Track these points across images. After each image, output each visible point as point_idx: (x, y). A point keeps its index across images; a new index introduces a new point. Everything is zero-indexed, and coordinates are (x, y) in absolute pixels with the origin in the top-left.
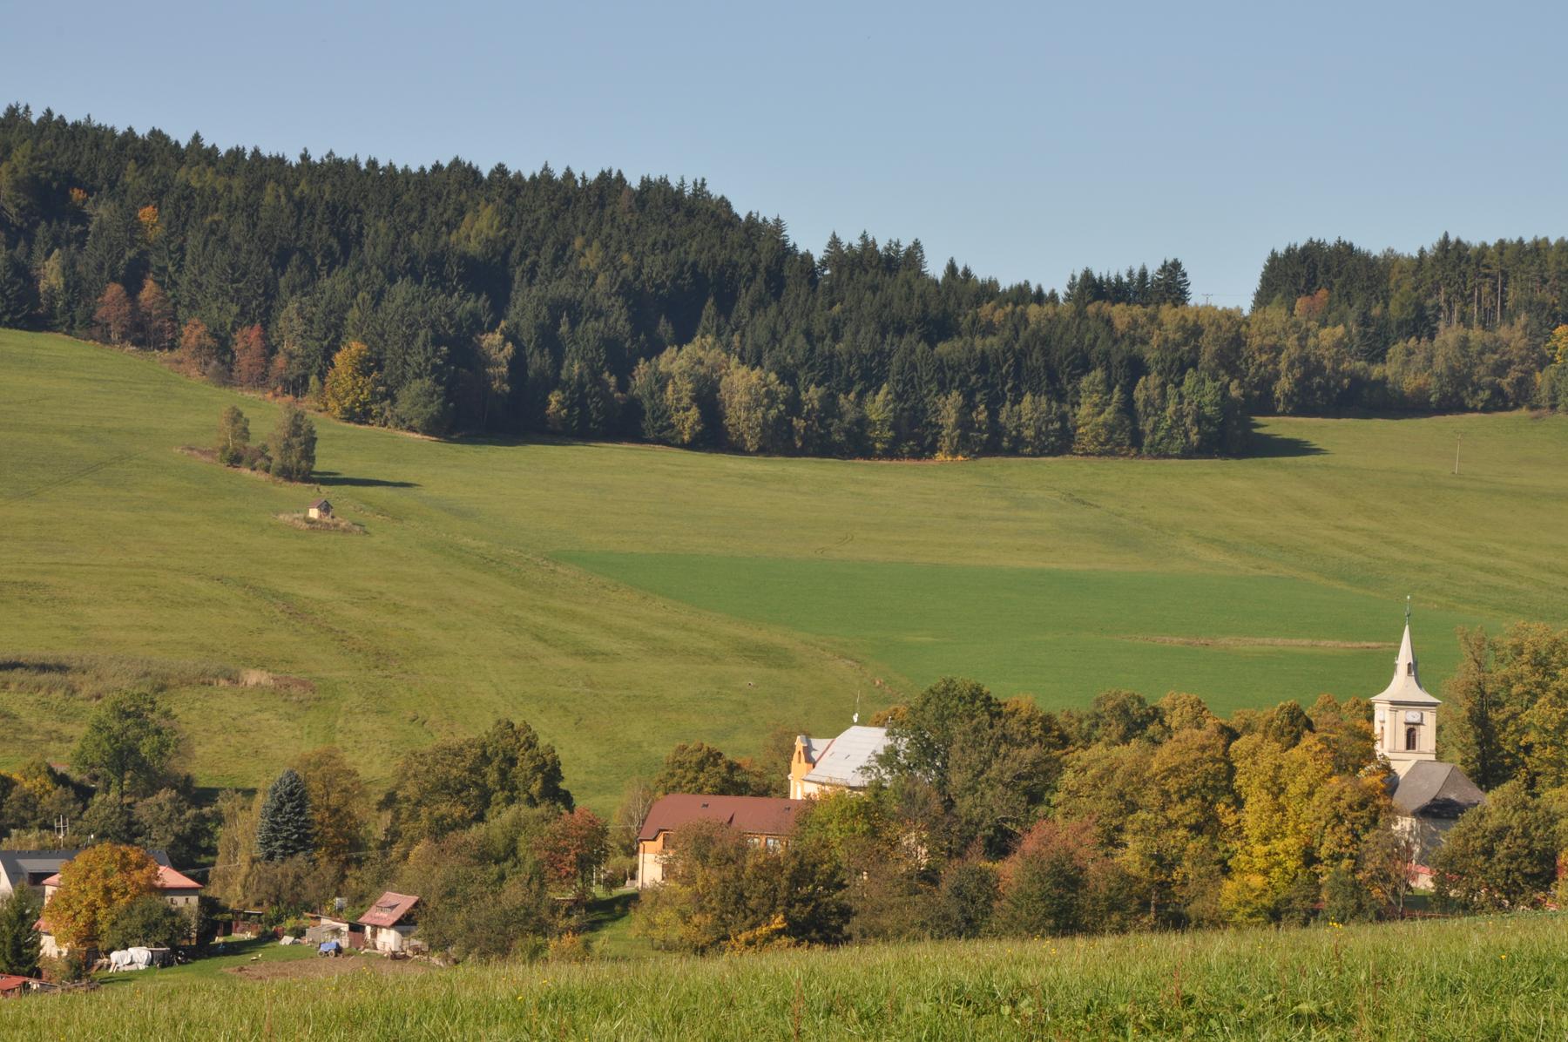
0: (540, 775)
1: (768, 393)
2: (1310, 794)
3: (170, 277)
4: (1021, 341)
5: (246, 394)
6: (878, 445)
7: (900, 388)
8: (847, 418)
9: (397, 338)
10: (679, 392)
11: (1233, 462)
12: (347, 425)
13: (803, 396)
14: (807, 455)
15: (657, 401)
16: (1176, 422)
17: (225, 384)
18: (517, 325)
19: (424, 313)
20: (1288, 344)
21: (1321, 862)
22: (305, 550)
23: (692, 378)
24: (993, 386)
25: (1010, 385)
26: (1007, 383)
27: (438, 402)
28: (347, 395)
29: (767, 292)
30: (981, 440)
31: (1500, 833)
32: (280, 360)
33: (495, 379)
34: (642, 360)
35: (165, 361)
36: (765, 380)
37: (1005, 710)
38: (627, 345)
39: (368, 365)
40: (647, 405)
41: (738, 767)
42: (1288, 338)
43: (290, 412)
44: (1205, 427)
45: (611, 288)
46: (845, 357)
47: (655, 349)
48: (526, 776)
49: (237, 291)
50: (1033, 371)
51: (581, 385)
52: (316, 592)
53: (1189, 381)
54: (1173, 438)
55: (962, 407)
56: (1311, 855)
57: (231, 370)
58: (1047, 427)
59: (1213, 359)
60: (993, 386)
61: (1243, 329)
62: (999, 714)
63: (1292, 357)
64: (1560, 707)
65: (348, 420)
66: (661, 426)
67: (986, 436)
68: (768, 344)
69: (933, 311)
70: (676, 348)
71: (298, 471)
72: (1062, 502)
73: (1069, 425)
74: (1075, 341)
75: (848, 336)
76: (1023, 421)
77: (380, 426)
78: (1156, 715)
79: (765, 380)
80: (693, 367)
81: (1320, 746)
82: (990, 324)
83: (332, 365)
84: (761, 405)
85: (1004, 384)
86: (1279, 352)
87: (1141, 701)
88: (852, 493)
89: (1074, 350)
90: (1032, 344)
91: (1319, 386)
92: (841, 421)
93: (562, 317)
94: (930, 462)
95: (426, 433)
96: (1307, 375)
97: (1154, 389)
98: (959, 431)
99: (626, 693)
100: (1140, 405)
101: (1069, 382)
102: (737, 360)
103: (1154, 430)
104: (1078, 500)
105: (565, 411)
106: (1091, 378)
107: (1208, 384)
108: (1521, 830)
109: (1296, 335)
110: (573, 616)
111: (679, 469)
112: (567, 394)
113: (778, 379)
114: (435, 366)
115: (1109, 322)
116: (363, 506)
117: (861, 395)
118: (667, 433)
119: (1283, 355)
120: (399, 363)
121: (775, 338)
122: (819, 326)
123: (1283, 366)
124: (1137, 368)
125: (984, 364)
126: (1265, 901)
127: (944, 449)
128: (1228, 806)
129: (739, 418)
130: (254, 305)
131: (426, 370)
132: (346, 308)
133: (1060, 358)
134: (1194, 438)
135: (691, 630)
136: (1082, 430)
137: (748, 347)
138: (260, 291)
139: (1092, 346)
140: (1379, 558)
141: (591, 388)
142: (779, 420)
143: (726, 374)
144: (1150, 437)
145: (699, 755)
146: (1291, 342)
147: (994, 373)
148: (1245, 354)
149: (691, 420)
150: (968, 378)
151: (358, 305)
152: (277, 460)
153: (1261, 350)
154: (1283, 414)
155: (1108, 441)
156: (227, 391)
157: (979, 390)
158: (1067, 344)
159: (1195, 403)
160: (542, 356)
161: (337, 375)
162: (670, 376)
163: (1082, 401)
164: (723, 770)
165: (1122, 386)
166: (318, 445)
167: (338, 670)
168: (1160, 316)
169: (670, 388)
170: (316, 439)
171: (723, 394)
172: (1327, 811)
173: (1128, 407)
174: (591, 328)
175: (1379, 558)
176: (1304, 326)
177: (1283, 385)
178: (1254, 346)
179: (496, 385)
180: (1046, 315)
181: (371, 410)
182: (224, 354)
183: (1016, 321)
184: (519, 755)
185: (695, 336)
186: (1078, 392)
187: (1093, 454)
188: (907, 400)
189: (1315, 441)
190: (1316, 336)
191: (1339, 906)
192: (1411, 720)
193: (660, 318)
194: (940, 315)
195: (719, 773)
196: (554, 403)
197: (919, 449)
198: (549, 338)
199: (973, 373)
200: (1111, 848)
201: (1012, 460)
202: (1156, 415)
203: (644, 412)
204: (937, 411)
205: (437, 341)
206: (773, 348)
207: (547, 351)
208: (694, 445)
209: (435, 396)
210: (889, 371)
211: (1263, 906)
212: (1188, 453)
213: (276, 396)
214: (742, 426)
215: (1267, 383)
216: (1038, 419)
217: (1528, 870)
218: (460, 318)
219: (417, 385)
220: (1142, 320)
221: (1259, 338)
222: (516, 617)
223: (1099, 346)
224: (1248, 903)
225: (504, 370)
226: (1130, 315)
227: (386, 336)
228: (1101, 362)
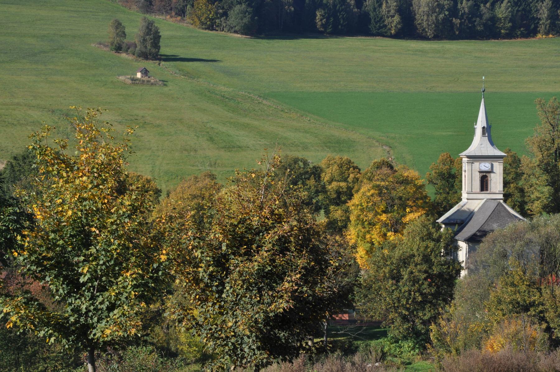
5: (157, 17)
6: (503, 31)
8: (484, 18)
14: (463, 38)
15: (377, 13)
22: (119, 95)
27: (248, 16)
31: (405, 261)
40: (372, 15)
43: (145, 22)
55: (551, 8)
66: (379, 26)
77: (221, 31)
81: (372, 191)
88: (476, 57)
94: (533, 39)
95: (242, 34)
98: (549, 21)
110: (245, 126)
112: (326, 11)
117: (493, 5)
118: (383, 30)
127: (541, 32)
129: (422, 20)
169: (384, 5)
197: (526, 32)
203: (370, 19)
204: (537, 11)
208: (398, 36)
209: (247, 14)
213: (171, 17)
214: (425, 24)
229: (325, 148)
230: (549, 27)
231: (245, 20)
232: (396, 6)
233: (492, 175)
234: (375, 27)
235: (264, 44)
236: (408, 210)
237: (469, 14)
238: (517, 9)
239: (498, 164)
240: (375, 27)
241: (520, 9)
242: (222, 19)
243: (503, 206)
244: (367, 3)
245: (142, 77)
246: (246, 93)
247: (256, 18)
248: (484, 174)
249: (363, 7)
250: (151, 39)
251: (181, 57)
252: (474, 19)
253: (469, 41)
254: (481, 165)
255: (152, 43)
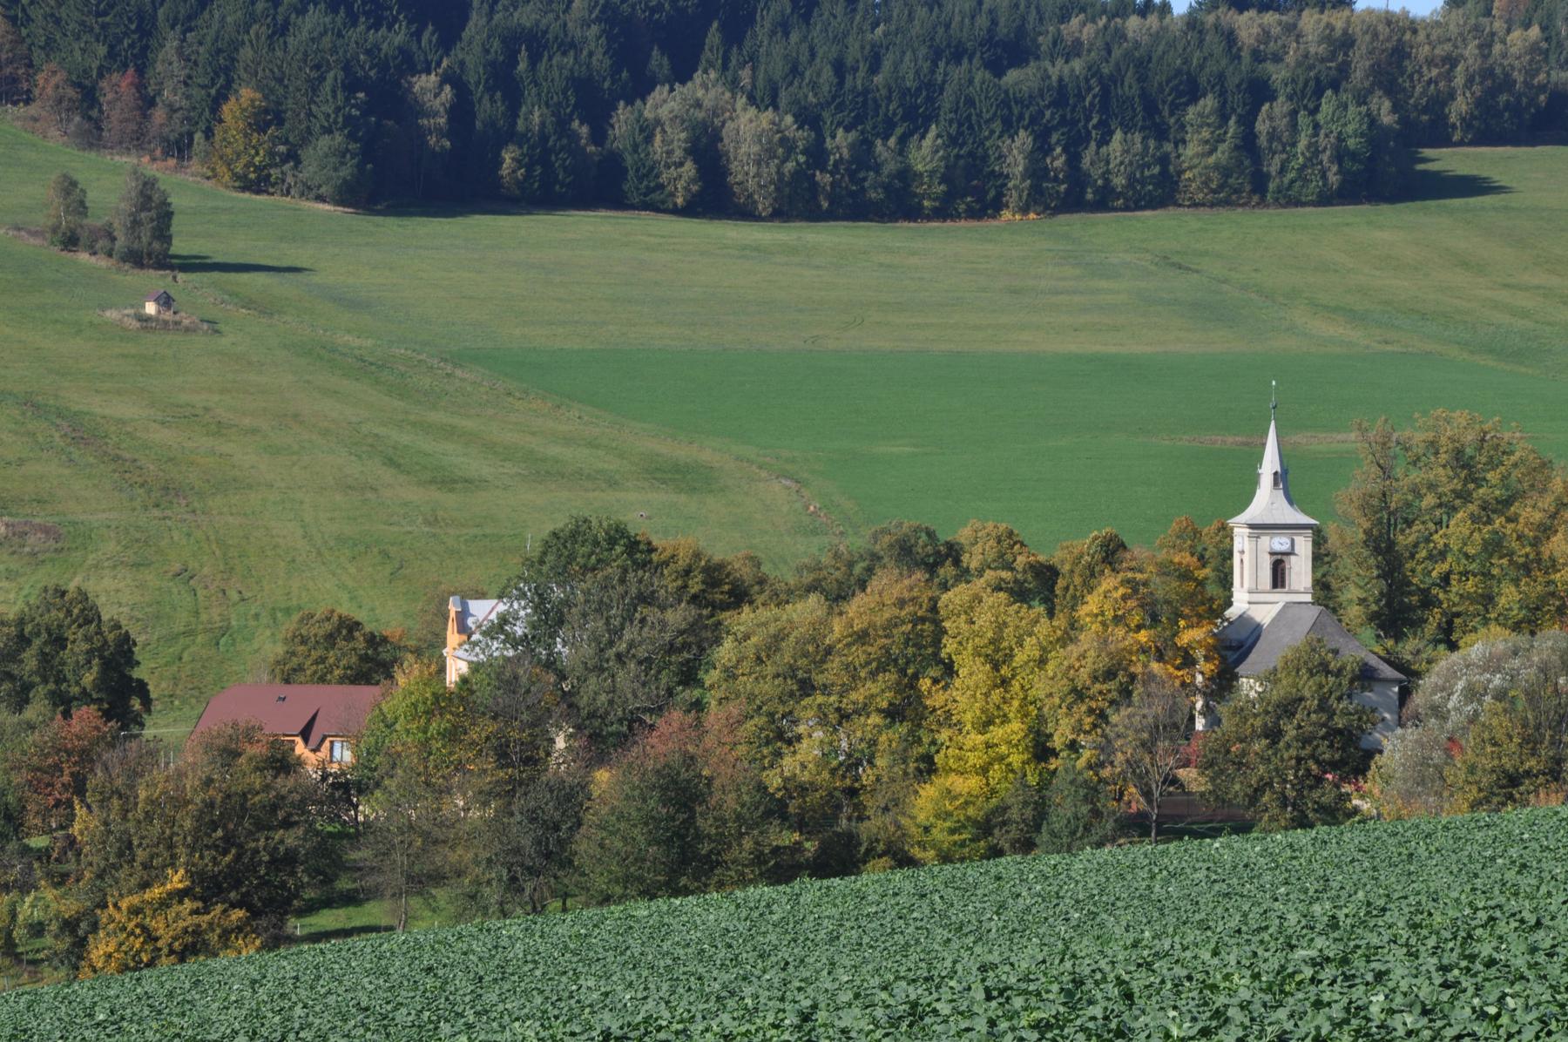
0: (96, 661)
1: (783, 141)
2: (1042, 662)
3: (24, 10)
4: (1113, 60)
5: (117, 158)
6: (926, 203)
7: (953, 130)
8: (886, 170)
9: (299, 82)
10: (671, 143)
11: (1385, 208)
12: (241, 195)
13: (829, 144)
15: (642, 155)
16: (1310, 159)
17: (91, 146)
18: (462, 63)
19: (334, 50)
20: (1467, 53)
21: (1056, 755)
22: (124, 356)
23: (686, 124)
24: (1074, 122)
25: (1095, 121)
26: (1092, 118)
28: (239, 156)
29: (792, 13)
30: (1058, 192)
32: (159, 115)
33: (431, 133)
34: (622, 103)
35: (18, 118)
36: (778, 125)
37: (654, 557)
38: (606, 85)
39: (265, 119)
40: (629, 160)
41: (385, 640)
42: (1466, 46)
43: (137, 179)
44: (1348, 164)
45: (591, 12)
46: (884, 92)
47: (641, 88)
48: (78, 662)
49: (104, 26)
50: (1124, 102)
51: (544, 138)
52: (126, 409)
53: (1327, 106)
54: (1306, 181)
56: (1044, 744)
57: (100, 129)
58: (1142, 172)
59: (1367, 77)
60: (1074, 122)
61: (1408, 36)
62: (644, 565)
63: (1471, 70)
64: (1485, 524)
65: (243, 189)
66: (647, 187)
67: (1063, 187)
68: (784, 79)
69: (1002, 31)
70: (667, 87)
71: (149, 255)
72: (1153, 268)
73: (1171, 168)
74: (1179, 62)
75: (887, 65)
76: (1111, 166)
78: (953, 553)
79: (778, 125)
80: (688, 110)
81: (1121, 591)
82: (1078, 43)
83: (221, 121)
84: (775, 157)
85: (1089, 119)
86: (1454, 65)
87: (931, 534)
88: (881, 265)
89: (1179, 72)
90: (1123, 68)
91: (1508, 104)
92: (878, 172)
93: (520, 52)
94: (994, 223)
96: (1492, 93)
97: (1281, 119)
99: (475, 531)
100: (1263, 141)
101: (1172, 114)
102: (744, 99)
103: (1283, 170)
104: (1173, 264)
105: (523, 170)
106: (1199, 108)
107: (1352, 109)
108: (1316, 702)
109: (1477, 42)
110: (449, 432)
111: (661, 240)
113: (796, 122)
114: (348, 119)
115: (1230, 37)
116: (226, 297)
117: (903, 140)
118: (656, 196)
119: (1459, 68)
120: (302, 115)
121: (795, 71)
122: (853, 52)
123: (1459, 80)
124: (1260, 92)
125: (1061, 95)
126: (971, 811)
128: (935, 681)
129: (747, 174)
130: (126, 45)
131: (335, 122)
132: (236, 46)
133: (1160, 84)
134: (1334, 179)
135: (597, 447)
136: (1188, 175)
137: (760, 83)
138: (133, 27)
139: (1201, 67)
140: (1549, 324)
141: (556, 141)
142: (798, 174)
143: (732, 119)
144: (1277, 180)
145: (328, 627)
146: (1471, 50)
147: (1075, 106)
148: (1410, 69)
149: (685, 177)
150: (1041, 113)
151: (251, 42)
152: (122, 241)
153: (1430, 62)
154: (1461, 143)
155: (1221, 187)
156: (93, 155)
157: (1055, 128)
158: (1169, 65)
159: (1335, 134)
160: (492, 100)
161: (226, 132)
162: (658, 122)
163: (1188, 137)
164: (360, 644)
165: (1240, 116)
166: (175, 220)
167: (104, 511)
168: (1301, 24)
169: (658, 138)
170: (172, 213)
171: (727, 144)
172: (1063, 685)
173: (1248, 143)
174: (559, 66)
175: (1549, 324)
176: (1488, 29)
177: (1460, 107)
178: (1421, 58)
179: (432, 140)
180: (1149, 29)
181: (269, 175)
182: (91, 107)
183: (1108, 38)
184: (69, 634)
185: (696, 70)
186: (1182, 127)
187: (1203, 205)
188: (964, 143)
189: (1498, 176)
190: (1503, 42)
191: (1069, 814)
192: (1278, 547)
193: (652, 49)
194: (1012, 35)
195: (355, 649)
196: (508, 161)
198: (503, 80)
199: (1048, 107)
200: (779, 744)
201: (1100, 216)
202: (1284, 151)
203: (626, 170)
205: (351, 85)
206: (791, 84)
207: (499, 94)
208: (692, 209)
209: (348, 156)
210: (939, 108)
211: (968, 818)
212: (1326, 199)
213: (154, 160)
214: (751, 184)
215: (1439, 103)
216: (1131, 163)
217: (1327, 756)
218: (386, 55)
219: (324, 142)
220: (1276, 31)
221: (1427, 47)
222: (377, 435)
223: (1211, 68)
224: (949, 814)
225: (442, 121)
226: (1260, 25)
227: (286, 82)
228: (1213, 87)
229: (657, 484)
230: (1029, 195)
231: (346, 172)
232: (686, 141)
233: (1292, 557)
234: (638, 189)
235: (392, 228)
236: (1182, 623)
237: (850, 162)
238: (956, 151)
240: (638, 189)
241: (962, 152)
242: (285, 168)
244: (617, 131)
245: (159, 312)
246: (409, 352)
247: (369, 166)
249: (609, 142)
250: (152, 220)
251: (216, 260)
252: (862, 175)
253: (850, 224)
255: (153, 228)
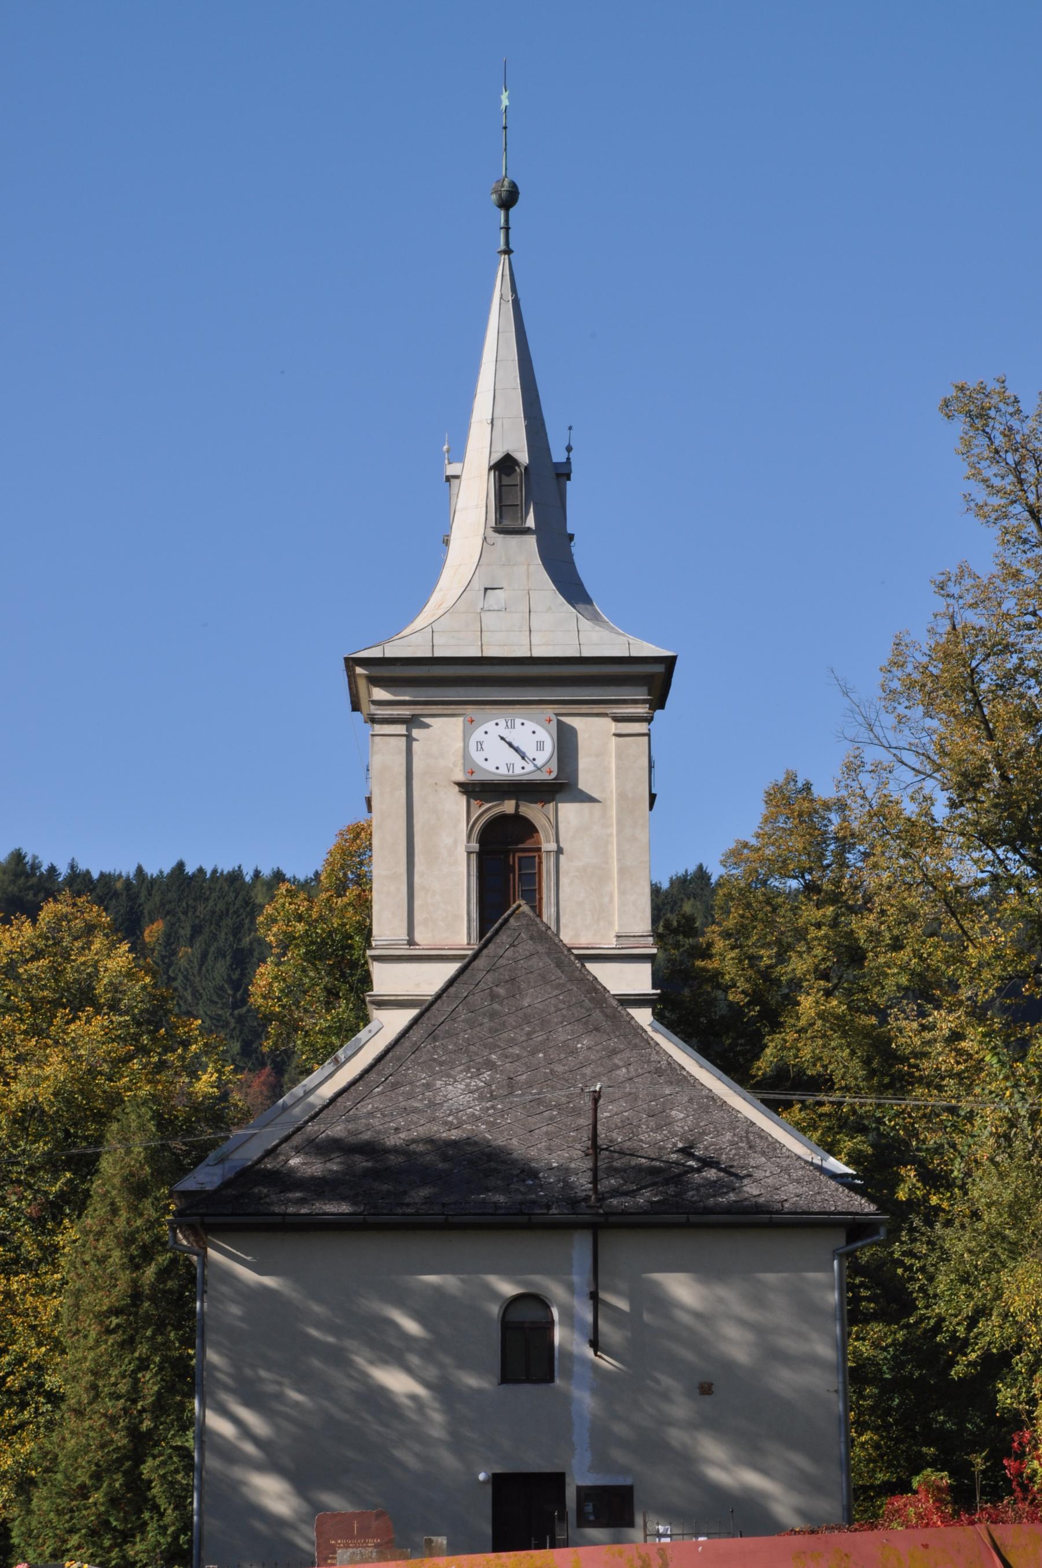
233: (568, 812)
239: (613, 727)
243: (648, 1042)
248: (509, 807)
254: (478, 735)
